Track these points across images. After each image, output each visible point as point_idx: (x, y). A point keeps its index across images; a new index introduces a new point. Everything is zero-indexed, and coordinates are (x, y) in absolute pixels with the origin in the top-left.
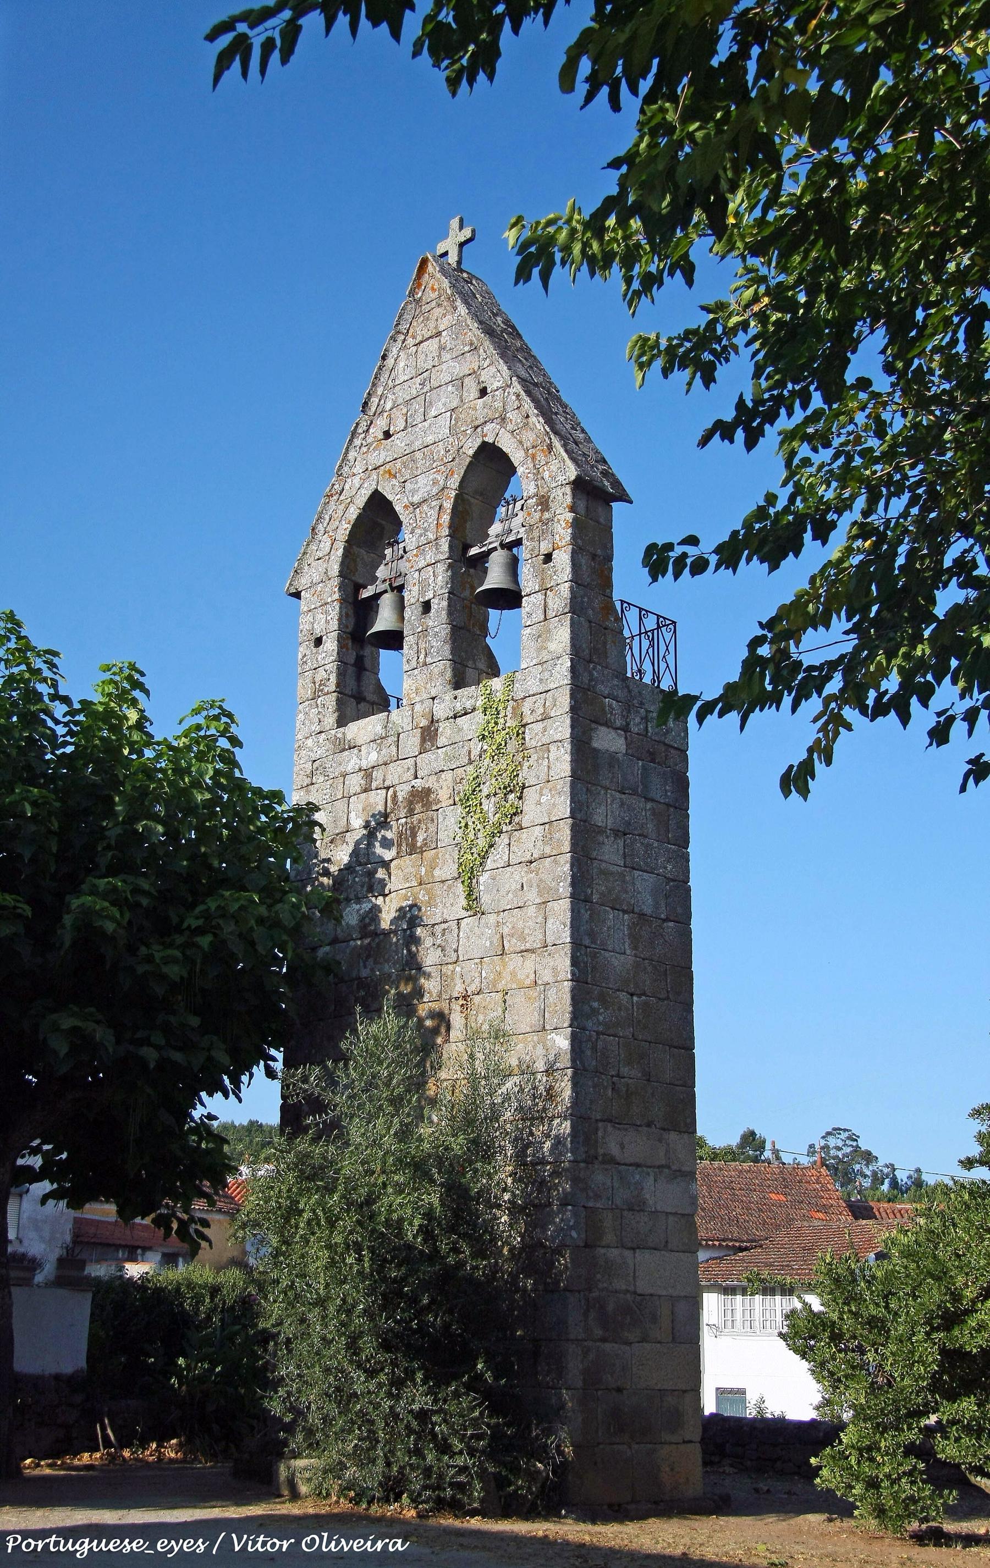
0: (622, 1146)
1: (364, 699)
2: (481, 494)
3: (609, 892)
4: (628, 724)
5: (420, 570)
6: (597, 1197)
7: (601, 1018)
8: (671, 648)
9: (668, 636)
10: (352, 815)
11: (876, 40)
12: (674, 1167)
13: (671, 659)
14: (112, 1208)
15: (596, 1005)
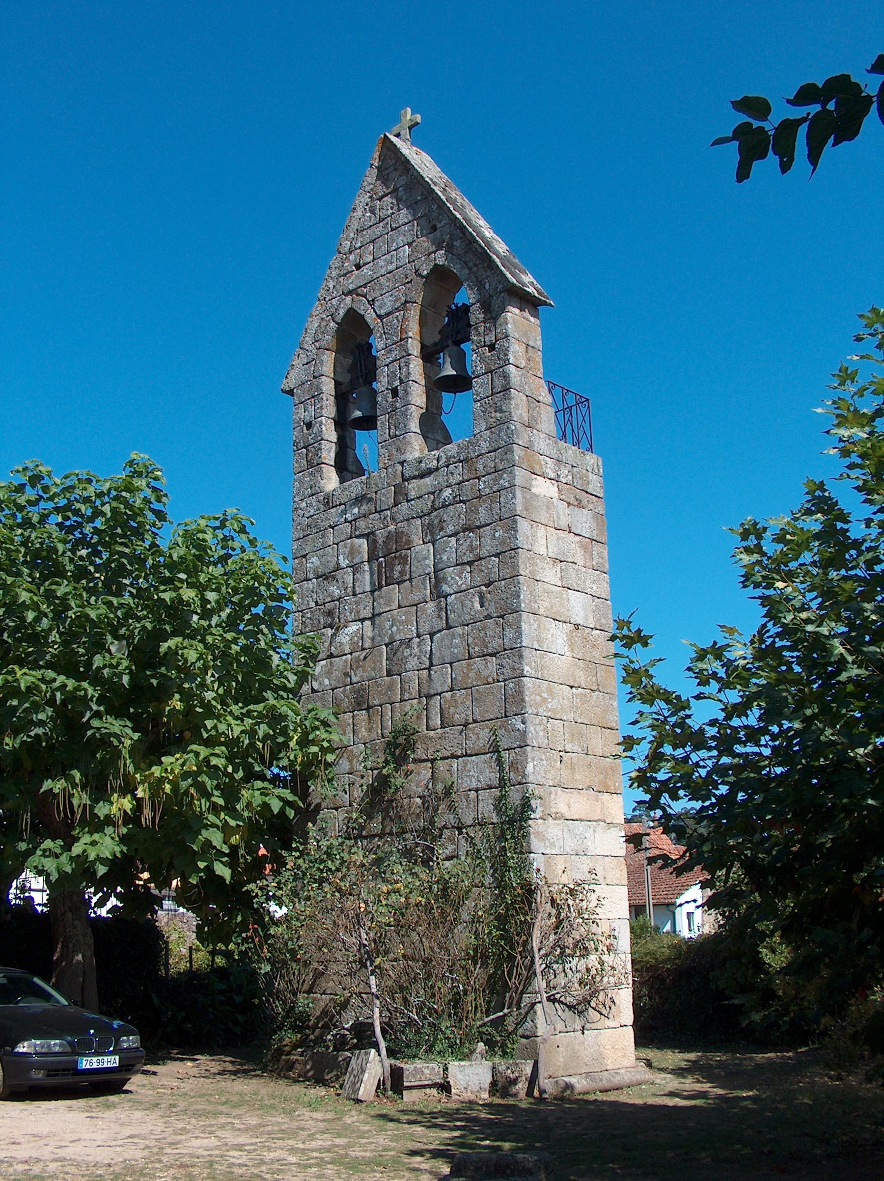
0: (569, 806)
1: (347, 470)
2: (434, 307)
3: (552, 607)
4: (559, 476)
5: (387, 365)
6: (553, 845)
7: (549, 706)
8: (587, 418)
9: (584, 410)
10: (341, 557)
11: (70, 779)
12: (607, 821)
13: (586, 427)
14: (50, 780)
15: (545, 695)
